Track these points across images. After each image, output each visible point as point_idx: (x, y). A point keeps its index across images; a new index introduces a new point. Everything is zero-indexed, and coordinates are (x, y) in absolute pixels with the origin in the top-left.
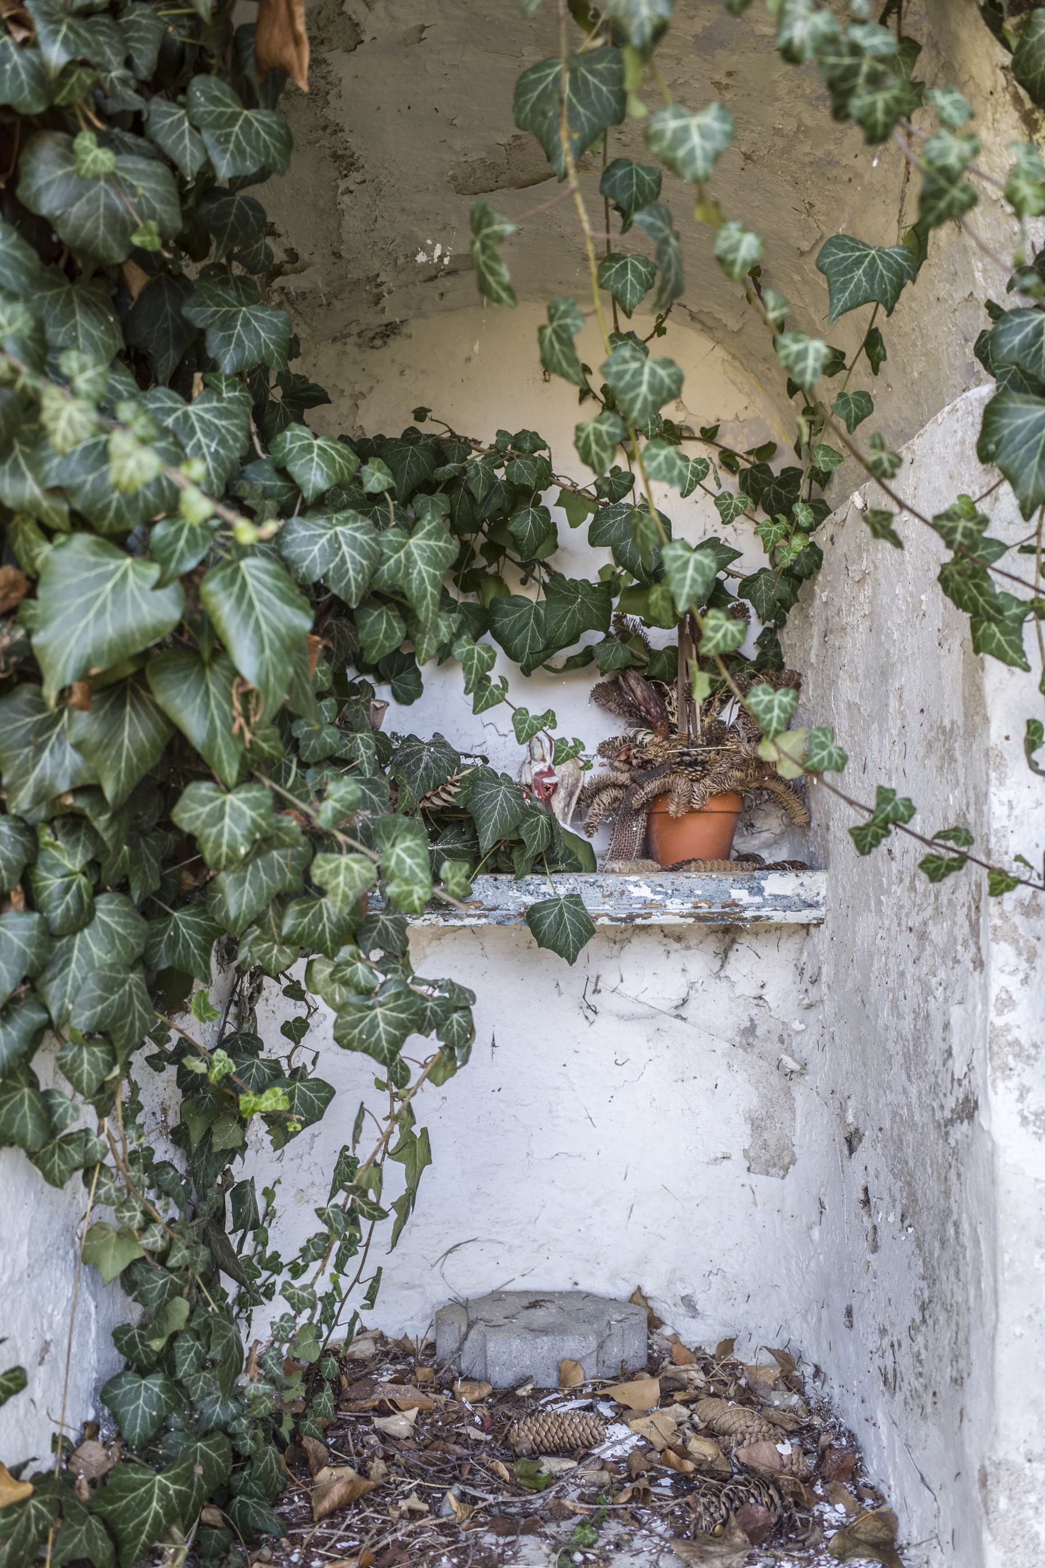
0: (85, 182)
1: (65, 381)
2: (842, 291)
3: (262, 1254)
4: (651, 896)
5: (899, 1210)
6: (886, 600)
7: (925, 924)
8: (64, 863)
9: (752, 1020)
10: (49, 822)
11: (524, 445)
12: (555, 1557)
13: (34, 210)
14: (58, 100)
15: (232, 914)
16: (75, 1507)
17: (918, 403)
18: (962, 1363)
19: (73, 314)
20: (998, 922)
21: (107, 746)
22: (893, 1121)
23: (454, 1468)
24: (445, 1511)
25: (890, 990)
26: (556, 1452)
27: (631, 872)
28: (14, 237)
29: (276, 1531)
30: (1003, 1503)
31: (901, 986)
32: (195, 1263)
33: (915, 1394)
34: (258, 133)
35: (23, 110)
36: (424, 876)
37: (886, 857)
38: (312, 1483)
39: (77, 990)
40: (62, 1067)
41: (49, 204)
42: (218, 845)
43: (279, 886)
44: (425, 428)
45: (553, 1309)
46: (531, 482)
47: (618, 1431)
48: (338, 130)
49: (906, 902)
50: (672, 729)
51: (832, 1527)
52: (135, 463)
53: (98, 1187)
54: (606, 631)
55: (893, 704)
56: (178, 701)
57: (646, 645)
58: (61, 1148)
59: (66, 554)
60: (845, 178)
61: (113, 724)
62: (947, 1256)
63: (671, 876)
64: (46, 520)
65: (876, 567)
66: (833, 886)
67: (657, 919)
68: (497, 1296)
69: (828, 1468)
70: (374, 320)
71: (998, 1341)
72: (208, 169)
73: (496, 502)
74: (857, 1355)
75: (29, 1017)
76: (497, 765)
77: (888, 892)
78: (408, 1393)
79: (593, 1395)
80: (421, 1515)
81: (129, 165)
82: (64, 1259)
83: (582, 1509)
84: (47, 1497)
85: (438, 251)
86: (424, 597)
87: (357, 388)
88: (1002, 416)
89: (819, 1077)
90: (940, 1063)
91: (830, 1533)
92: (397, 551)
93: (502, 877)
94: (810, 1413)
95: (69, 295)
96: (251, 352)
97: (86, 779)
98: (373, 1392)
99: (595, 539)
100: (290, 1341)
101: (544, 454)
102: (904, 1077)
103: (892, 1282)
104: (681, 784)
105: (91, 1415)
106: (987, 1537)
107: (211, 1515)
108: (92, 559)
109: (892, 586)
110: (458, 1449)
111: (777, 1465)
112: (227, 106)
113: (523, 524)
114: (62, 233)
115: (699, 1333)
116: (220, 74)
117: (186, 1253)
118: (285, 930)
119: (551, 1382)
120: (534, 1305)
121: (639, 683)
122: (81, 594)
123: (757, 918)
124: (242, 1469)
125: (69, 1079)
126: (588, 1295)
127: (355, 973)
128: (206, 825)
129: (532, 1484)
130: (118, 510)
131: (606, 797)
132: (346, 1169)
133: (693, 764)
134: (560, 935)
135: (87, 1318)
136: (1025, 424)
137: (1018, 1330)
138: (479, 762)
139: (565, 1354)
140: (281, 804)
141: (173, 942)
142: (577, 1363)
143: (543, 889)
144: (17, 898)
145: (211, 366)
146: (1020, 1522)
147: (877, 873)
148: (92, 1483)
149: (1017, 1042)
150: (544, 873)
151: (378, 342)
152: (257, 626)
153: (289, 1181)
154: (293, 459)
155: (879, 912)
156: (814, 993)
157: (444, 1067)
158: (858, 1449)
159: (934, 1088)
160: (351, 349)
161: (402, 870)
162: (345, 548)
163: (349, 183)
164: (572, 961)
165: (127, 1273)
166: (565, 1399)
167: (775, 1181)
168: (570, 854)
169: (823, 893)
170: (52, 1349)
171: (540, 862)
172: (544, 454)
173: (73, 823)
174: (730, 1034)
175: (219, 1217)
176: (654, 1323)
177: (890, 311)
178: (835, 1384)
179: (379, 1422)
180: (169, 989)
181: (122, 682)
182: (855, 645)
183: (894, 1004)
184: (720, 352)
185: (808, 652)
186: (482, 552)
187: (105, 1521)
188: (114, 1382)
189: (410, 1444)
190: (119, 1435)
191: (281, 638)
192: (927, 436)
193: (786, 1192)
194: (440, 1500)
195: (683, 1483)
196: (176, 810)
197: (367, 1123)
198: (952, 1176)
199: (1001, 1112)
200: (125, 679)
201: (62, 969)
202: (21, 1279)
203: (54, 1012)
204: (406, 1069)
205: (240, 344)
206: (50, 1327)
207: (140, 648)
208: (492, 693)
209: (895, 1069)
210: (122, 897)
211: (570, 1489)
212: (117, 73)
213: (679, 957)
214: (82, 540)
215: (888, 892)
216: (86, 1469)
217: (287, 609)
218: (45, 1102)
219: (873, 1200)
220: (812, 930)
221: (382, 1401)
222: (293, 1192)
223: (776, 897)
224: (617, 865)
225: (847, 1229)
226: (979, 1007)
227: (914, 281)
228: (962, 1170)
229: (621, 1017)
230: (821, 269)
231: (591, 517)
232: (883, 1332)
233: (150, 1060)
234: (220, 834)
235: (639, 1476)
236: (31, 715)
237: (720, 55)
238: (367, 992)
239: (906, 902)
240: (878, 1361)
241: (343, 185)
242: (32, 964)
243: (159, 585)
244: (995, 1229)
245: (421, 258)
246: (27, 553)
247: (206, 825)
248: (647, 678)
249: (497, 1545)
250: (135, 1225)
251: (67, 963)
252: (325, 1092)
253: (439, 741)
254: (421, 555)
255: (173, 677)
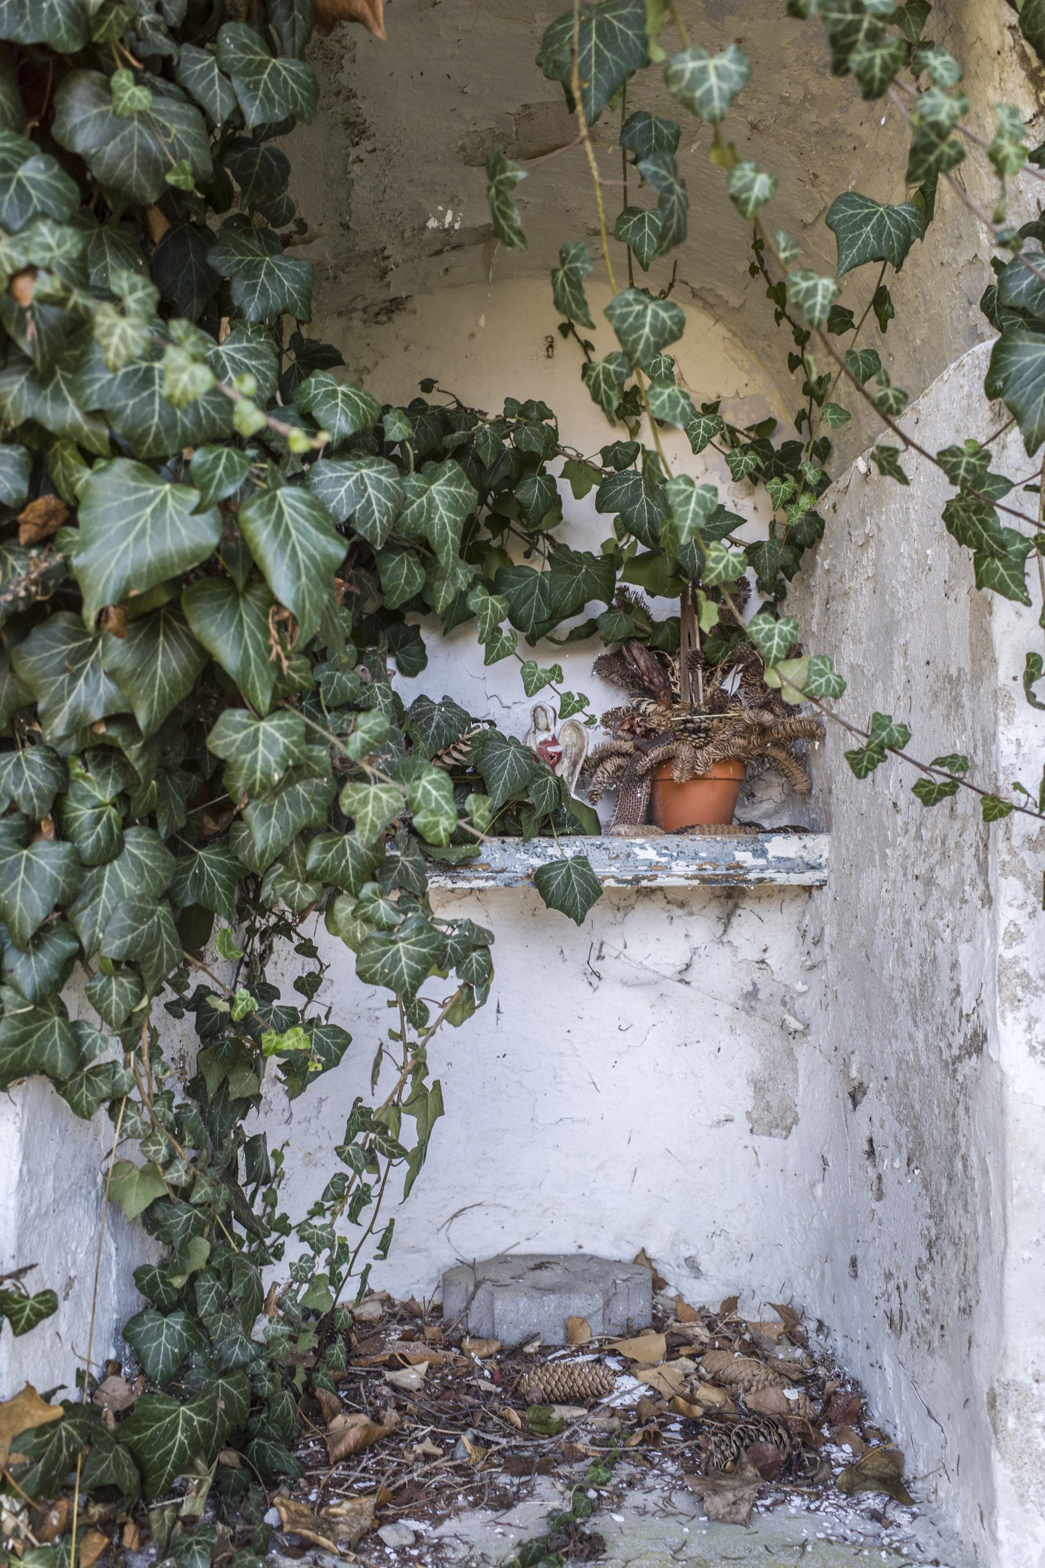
0: (119, 121)
1: (116, 300)
2: (850, 247)
3: (270, 1216)
4: (657, 858)
5: (905, 1155)
6: (890, 559)
7: (932, 870)
8: (94, 794)
9: (754, 984)
10: (80, 754)
11: (532, 414)
12: (569, 1494)
13: (68, 148)
14: (96, 38)
15: (258, 848)
16: (102, 1435)
17: (920, 370)
18: (970, 1293)
19: (103, 256)
20: (1007, 857)
21: (141, 674)
22: (899, 1068)
23: (467, 1415)
24: (460, 1453)
25: (895, 940)
26: (566, 1400)
27: (636, 835)
28: (56, 168)
29: (293, 1472)
30: (1011, 1423)
31: (907, 934)
32: (216, 1201)
33: (922, 1331)
34: (285, 81)
35: (59, 49)
36: (450, 808)
37: (892, 811)
38: (327, 1430)
39: (108, 919)
40: (90, 998)
41: (84, 142)
42: (252, 772)
43: (305, 821)
44: (432, 399)
45: (559, 1270)
46: (539, 449)
47: (626, 1382)
48: (351, 95)
49: (912, 852)
50: (674, 698)
51: (839, 1465)
52: (184, 374)
53: (124, 1121)
54: (609, 603)
55: (898, 660)
56: (213, 630)
57: (649, 617)
58: (88, 1080)
59: (107, 478)
60: (850, 147)
61: (147, 652)
62: (955, 1191)
63: (676, 839)
64: (86, 445)
65: (879, 529)
66: (835, 849)
67: (662, 881)
68: (502, 1260)
69: (835, 1411)
70: (378, 295)
71: (1007, 1266)
73: (503, 469)
74: (862, 1304)
75: (59, 946)
76: (506, 728)
77: (893, 845)
78: (416, 1349)
79: (600, 1350)
80: (435, 1457)
81: (162, 107)
82: (87, 1199)
83: (595, 1452)
84: (78, 1420)
85: (449, 218)
86: (446, 542)
87: (363, 363)
88: (1011, 354)
90: (947, 1003)
91: (838, 1471)
92: (420, 496)
93: (509, 840)
94: (815, 1364)
95: (99, 236)
96: (275, 301)
97: (120, 707)
98: (382, 1348)
99: (602, 506)
100: (309, 1281)
101: (552, 423)
102: (910, 1023)
103: (903, 1216)
104: (685, 751)
105: (112, 1355)
106: (995, 1455)
107: (229, 1457)
108: (133, 484)
109: (897, 545)
110: (469, 1399)
111: (784, 1408)
112: (256, 53)
113: (530, 493)
114: (96, 172)
115: (702, 1293)
116: (248, 19)
117: (209, 1190)
118: (310, 865)
119: (558, 1339)
120: (540, 1267)
121: (639, 655)
122: (122, 518)
123: (761, 880)
124: (260, 1412)
125: (98, 1010)
126: (592, 1257)
127: (377, 909)
128: (240, 751)
129: (544, 1429)
130: (157, 435)
131: (610, 766)
132: (360, 1118)
133: (696, 731)
134: (568, 896)
135: (109, 1259)
136: (1033, 362)
137: (1026, 1255)
138: (487, 726)
139: (572, 1311)
140: (310, 737)
141: (198, 880)
142: (584, 1320)
143: (550, 851)
144: (48, 829)
145: (237, 315)
146: (1028, 1441)
147: (882, 827)
148: (118, 1416)
149: (1025, 974)
150: (552, 836)
151: (383, 318)
152: (292, 550)
153: (300, 1133)
154: (318, 405)
155: (884, 866)
156: (817, 955)
157: (462, 1008)
158: (862, 1395)
159: (941, 1030)
160: (356, 323)
161: (428, 802)
162: (370, 490)
163: (360, 151)
164: (580, 921)
165: (149, 1211)
166: (572, 1355)
167: (777, 1142)
168: (574, 821)
169: (826, 855)
170: (76, 1285)
171: (548, 826)
172: (552, 423)
173: (105, 755)
174: (733, 998)
175: (232, 1171)
176: (658, 1284)
177: (899, 266)
178: (838, 1335)
179: (389, 1375)
180: (192, 928)
181: (157, 609)
182: (859, 610)
183: (900, 954)
184: (720, 330)
185: (808, 622)
186: (487, 525)
187: (130, 1450)
188: (136, 1320)
189: (421, 1394)
190: (142, 1372)
191: (316, 565)
192: (932, 395)
193: (790, 1151)
194: (454, 1446)
195: (692, 1427)
196: (211, 737)
197: (386, 1065)
198: (961, 1111)
199: (1009, 1044)
200: (156, 610)
201: (92, 899)
202: (46, 1213)
203: (85, 941)
204: (424, 1009)
205: (264, 292)
206: (74, 1263)
207: (179, 572)
208: (503, 645)
209: (901, 1017)
210: (150, 831)
211: (582, 1434)
212: (147, 18)
213: (682, 922)
214: (122, 465)
215: (893, 845)
216: (110, 1403)
217: (322, 537)
218: (74, 1034)
219: (878, 1149)
220: (815, 892)
221: (393, 1356)
222: (301, 1155)
223: (779, 859)
224: (623, 829)
225: (850, 1182)
226: (988, 942)
227: (922, 238)
228: (970, 1103)
229: (625, 984)
230: (830, 226)
231: (595, 488)
232: (889, 1276)
233: (168, 1006)
234: (254, 760)
235: (648, 1422)
236: (66, 643)
237: (730, 21)
238: (390, 928)
239: (912, 852)
240: (883, 1305)
241: (354, 153)
242: (64, 892)
243: (198, 510)
244: (1004, 1157)
245: (432, 223)
246: (66, 479)
247: (240, 751)
248: (650, 649)
249: (512, 1484)
250: (161, 1159)
251: (98, 893)
252: (342, 1039)
253: (448, 702)
254: (442, 500)
255: (207, 606)
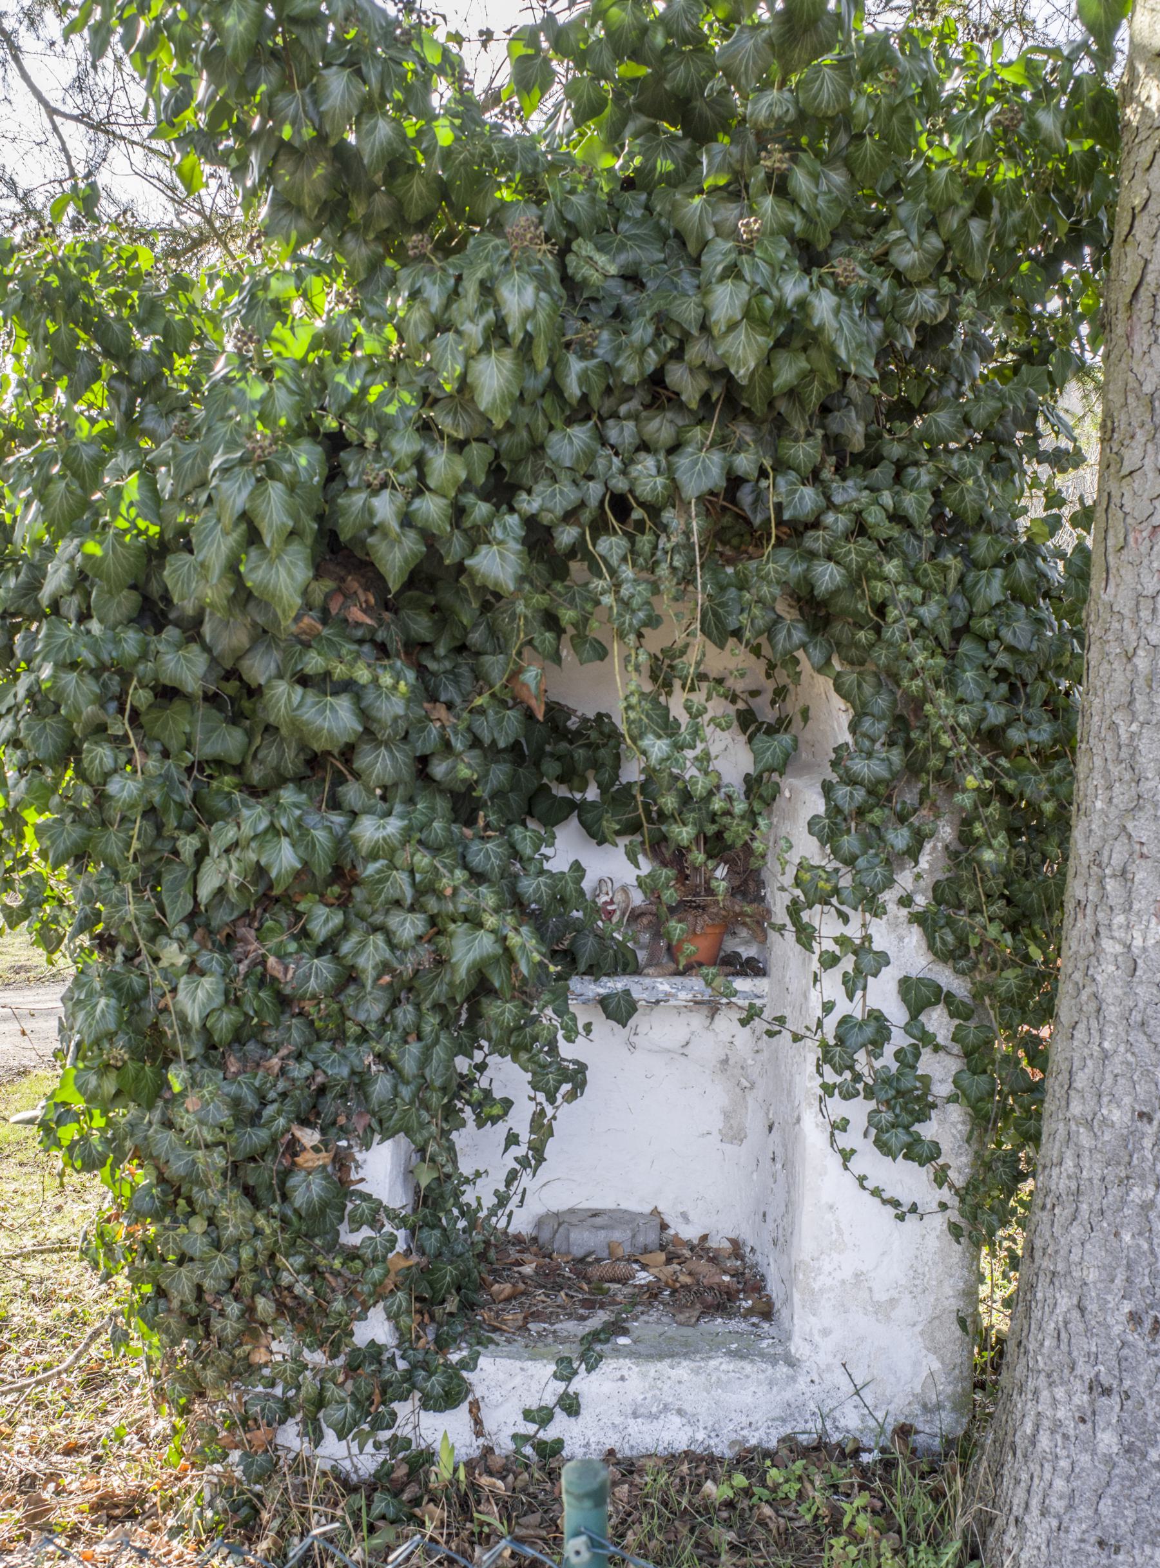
47: (643, 1274)
68: (572, 1211)
72: (494, 742)
89: (759, 1093)
115: (690, 1233)
119: (605, 1255)
157: (572, 1096)
176: (664, 1227)
195: (674, 1292)
